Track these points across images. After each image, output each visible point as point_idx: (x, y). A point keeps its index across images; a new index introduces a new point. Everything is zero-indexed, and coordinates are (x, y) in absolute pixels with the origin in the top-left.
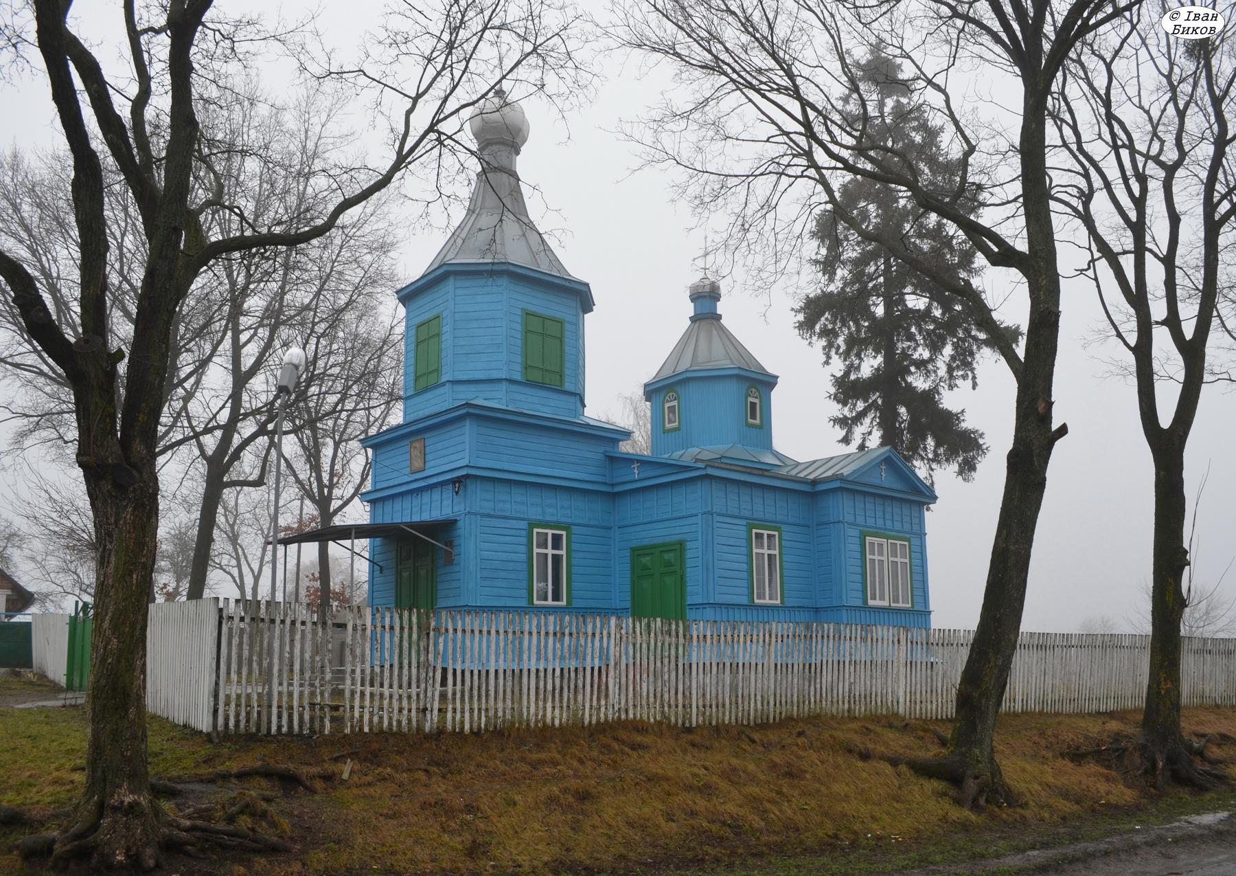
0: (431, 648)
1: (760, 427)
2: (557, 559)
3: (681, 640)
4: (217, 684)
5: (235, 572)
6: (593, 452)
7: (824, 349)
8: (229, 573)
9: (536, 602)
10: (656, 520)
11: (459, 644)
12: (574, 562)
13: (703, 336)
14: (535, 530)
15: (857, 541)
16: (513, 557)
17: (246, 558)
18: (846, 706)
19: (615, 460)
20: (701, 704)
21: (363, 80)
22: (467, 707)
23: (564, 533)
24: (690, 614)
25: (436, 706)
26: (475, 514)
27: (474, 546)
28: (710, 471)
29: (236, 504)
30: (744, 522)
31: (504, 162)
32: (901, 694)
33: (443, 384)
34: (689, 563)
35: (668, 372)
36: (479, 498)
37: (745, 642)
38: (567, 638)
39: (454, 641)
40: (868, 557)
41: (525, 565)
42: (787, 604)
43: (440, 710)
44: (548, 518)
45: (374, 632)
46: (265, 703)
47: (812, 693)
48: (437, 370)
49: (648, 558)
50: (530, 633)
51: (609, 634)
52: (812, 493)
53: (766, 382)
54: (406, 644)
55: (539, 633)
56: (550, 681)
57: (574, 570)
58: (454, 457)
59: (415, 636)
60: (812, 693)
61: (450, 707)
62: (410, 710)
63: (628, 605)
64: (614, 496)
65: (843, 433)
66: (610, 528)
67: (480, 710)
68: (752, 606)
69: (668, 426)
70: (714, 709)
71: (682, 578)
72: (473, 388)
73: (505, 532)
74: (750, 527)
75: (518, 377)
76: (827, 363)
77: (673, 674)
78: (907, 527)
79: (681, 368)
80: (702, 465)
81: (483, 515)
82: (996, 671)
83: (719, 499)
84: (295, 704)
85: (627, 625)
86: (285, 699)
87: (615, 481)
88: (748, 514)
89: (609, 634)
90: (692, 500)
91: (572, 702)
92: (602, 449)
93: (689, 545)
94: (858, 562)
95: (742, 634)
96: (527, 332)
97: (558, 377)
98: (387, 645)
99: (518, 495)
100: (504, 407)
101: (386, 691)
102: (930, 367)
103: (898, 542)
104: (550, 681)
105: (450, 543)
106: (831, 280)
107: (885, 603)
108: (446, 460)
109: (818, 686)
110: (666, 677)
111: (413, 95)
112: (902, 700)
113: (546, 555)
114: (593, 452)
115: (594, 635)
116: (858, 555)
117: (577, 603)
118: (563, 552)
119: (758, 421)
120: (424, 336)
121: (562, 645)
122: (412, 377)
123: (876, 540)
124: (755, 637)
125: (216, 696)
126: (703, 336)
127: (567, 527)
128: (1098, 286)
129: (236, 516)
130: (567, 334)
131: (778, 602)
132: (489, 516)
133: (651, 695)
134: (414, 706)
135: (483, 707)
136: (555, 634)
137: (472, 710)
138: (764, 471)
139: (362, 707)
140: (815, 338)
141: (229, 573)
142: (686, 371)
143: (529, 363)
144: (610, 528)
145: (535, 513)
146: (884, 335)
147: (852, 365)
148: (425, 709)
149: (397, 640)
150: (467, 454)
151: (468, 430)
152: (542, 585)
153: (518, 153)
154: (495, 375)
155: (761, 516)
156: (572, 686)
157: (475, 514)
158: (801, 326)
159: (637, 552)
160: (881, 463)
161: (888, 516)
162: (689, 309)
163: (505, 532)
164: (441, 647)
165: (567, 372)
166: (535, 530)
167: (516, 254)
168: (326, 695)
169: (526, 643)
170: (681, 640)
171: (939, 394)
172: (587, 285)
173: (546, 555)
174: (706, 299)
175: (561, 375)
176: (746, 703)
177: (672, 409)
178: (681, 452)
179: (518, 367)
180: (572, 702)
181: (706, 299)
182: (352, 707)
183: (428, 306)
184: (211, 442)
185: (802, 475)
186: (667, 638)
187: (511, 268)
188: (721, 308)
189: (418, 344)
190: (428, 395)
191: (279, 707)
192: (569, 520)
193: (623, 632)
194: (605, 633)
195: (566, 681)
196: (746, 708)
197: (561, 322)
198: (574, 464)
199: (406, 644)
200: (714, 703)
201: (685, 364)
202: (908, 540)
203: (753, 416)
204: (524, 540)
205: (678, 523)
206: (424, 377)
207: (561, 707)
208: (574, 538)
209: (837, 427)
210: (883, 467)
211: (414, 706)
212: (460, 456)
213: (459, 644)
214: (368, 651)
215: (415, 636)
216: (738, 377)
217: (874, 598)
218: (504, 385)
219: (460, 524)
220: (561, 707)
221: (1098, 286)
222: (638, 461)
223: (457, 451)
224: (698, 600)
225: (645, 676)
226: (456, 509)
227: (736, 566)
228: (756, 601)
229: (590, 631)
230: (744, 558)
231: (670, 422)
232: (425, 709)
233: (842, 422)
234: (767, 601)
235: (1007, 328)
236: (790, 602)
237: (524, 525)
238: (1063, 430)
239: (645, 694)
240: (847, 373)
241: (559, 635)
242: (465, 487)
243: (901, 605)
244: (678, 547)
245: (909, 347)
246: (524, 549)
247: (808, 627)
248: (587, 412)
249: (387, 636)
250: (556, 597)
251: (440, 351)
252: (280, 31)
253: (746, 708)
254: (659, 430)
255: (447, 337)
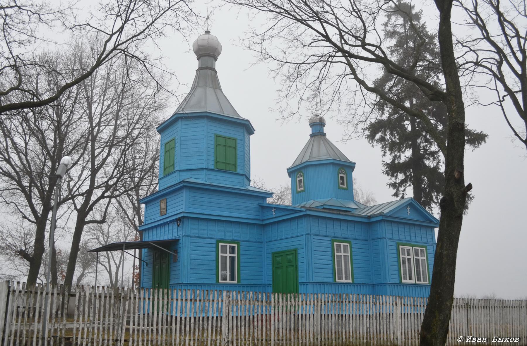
0: (121, 308)
1: (346, 189)
2: (232, 259)
3: (265, 303)
4: (5, 325)
5: (107, 265)
6: (252, 204)
7: (382, 147)
8: (104, 265)
9: (220, 281)
10: (284, 238)
11: (137, 305)
12: (242, 260)
13: (316, 144)
14: (220, 244)
15: (395, 248)
16: (209, 258)
17: (113, 258)
18: (365, 341)
19: (265, 208)
20: (276, 338)
21: (88, 28)
22: (140, 339)
23: (236, 245)
24: (301, 289)
25: (123, 338)
26: (188, 236)
27: (187, 253)
28: (308, 212)
29: (108, 232)
30: (329, 239)
31: (209, 65)
32: (399, 334)
33: (175, 172)
34: (300, 260)
35: (298, 163)
36: (190, 228)
37: (302, 305)
38: (198, 302)
39: (134, 303)
40: (401, 256)
41: (215, 262)
42: (355, 282)
43: (125, 341)
44: (227, 238)
45: (90, 300)
46: (30, 335)
47: (344, 333)
48: (173, 165)
49: (280, 258)
50: (177, 300)
51: (222, 301)
52: (370, 224)
53: (350, 167)
54: (107, 305)
55: (182, 299)
56: (188, 326)
57: (242, 264)
58: (178, 208)
59: (112, 301)
60: (344, 333)
61: (131, 339)
62: (108, 341)
63: (271, 282)
64: (264, 226)
65: (395, 191)
66: (262, 243)
67: (148, 341)
68: (335, 283)
69: (299, 190)
70: (284, 342)
71: (296, 268)
72: (189, 173)
73: (204, 245)
74: (333, 242)
75: (212, 167)
76: (384, 155)
77: (260, 322)
78: (424, 240)
79: (304, 161)
80: (304, 209)
81: (192, 237)
82: (440, 323)
83: (314, 227)
84: (46, 336)
85: (233, 296)
86: (41, 334)
87: (265, 218)
88: (332, 234)
89: (222, 301)
90: (301, 228)
91: (201, 337)
92: (257, 202)
93: (299, 251)
94: (396, 259)
95: (300, 300)
96: (217, 145)
97: (234, 167)
98: (97, 306)
99: (211, 226)
100: (204, 182)
101: (136, 327)
102: (435, 156)
103: (419, 248)
104: (188, 326)
105: (176, 251)
106: (383, 113)
107: (413, 281)
108: (176, 209)
109: (347, 329)
110: (256, 324)
111: (111, 33)
112: (399, 337)
113: (226, 257)
114: (252, 204)
115: (213, 301)
116: (395, 256)
117: (243, 282)
118: (236, 255)
119: (345, 186)
120: (168, 148)
121: (195, 306)
122: (163, 169)
123: (406, 248)
124: (308, 302)
125: (4, 332)
126: (316, 144)
127: (238, 242)
128: (503, 109)
129: (108, 238)
130: (238, 146)
131: (350, 281)
132: (195, 237)
133: (247, 334)
134: (111, 338)
135: (150, 339)
136: (191, 300)
137: (143, 341)
138: (348, 212)
139: (82, 338)
140: (375, 143)
141: (104, 265)
142: (306, 162)
143: (218, 160)
144: (262, 243)
145: (220, 235)
146: (408, 139)
147: (396, 156)
148: (117, 340)
149: (102, 303)
150: (184, 206)
151: (184, 195)
152: (224, 272)
153: (216, 60)
154: (200, 166)
155: (339, 235)
156: (201, 328)
157: (188, 236)
158: (368, 137)
159: (275, 255)
160: (407, 206)
161: (413, 234)
162: (309, 131)
163: (204, 245)
164: (127, 307)
165: (238, 164)
166: (220, 244)
167: (212, 108)
168: (63, 332)
169: (174, 305)
170: (265, 303)
171: (439, 169)
172: (248, 121)
173: (226, 257)
174: (318, 126)
175: (235, 166)
176: (304, 338)
177: (300, 181)
178: (305, 203)
179: (213, 163)
180: (201, 337)
181: (318, 126)
182: (77, 339)
183: (170, 134)
184: (80, 201)
185: (365, 214)
186: (256, 302)
187: (208, 115)
188: (326, 130)
189: (166, 152)
190: (169, 177)
191: (37, 338)
192: (239, 239)
193: (231, 299)
194: (220, 299)
195: (197, 326)
196: (304, 341)
197: (235, 140)
198: (243, 210)
199: (107, 305)
200: (284, 338)
201: (306, 158)
202: (425, 247)
203: (343, 184)
204: (214, 249)
205: (294, 239)
206: (168, 170)
207: (194, 340)
208: (242, 248)
209: (391, 188)
210: (409, 208)
211: (111, 338)
212: (181, 207)
213: (137, 305)
214: (86, 309)
215: (112, 301)
216: (333, 164)
217: (405, 278)
218: (205, 172)
219: (181, 241)
220: (194, 340)
221: (503, 109)
222: (275, 208)
223: (179, 205)
224: (304, 280)
225: (243, 323)
226: (179, 233)
227: (326, 262)
228: (337, 281)
229: (211, 300)
230: (330, 258)
231: (300, 187)
232: (117, 340)
233: (394, 185)
234: (344, 281)
235: (477, 133)
236: (357, 281)
237: (214, 241)
238: (470, 187)
239: (243, 333)
240: (394, 160)
241: (193, 301)
242: (183, 222)
243: (422, 282)
244: (294, 252)
245: (427, 146)
246: (214, 254)
247: (340, 296)
248: (252, 184)
249: (97, 301)
250: (232, 278)
251: (174, 155)
252: (62, 8)
253: (304, 341)
254: (295, 192)
255: (177, 149)
